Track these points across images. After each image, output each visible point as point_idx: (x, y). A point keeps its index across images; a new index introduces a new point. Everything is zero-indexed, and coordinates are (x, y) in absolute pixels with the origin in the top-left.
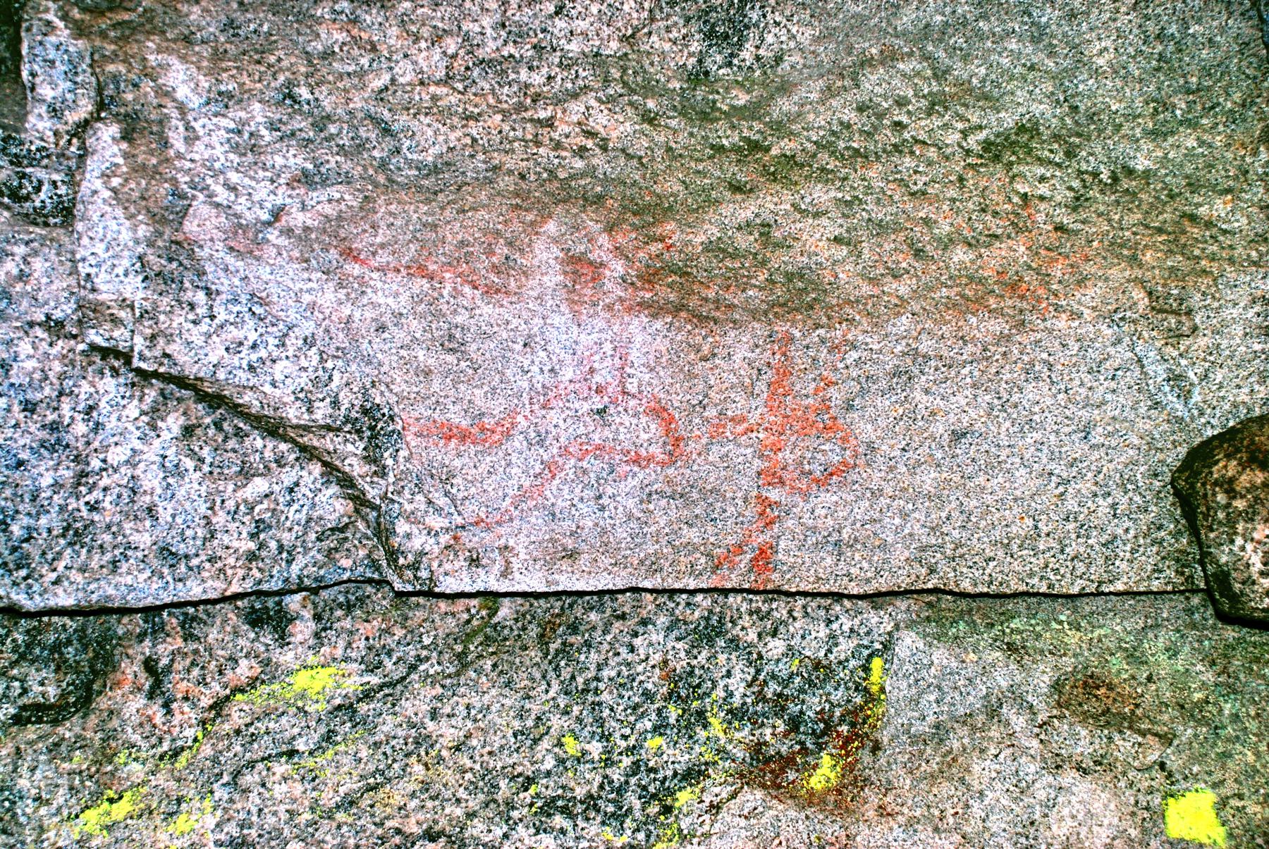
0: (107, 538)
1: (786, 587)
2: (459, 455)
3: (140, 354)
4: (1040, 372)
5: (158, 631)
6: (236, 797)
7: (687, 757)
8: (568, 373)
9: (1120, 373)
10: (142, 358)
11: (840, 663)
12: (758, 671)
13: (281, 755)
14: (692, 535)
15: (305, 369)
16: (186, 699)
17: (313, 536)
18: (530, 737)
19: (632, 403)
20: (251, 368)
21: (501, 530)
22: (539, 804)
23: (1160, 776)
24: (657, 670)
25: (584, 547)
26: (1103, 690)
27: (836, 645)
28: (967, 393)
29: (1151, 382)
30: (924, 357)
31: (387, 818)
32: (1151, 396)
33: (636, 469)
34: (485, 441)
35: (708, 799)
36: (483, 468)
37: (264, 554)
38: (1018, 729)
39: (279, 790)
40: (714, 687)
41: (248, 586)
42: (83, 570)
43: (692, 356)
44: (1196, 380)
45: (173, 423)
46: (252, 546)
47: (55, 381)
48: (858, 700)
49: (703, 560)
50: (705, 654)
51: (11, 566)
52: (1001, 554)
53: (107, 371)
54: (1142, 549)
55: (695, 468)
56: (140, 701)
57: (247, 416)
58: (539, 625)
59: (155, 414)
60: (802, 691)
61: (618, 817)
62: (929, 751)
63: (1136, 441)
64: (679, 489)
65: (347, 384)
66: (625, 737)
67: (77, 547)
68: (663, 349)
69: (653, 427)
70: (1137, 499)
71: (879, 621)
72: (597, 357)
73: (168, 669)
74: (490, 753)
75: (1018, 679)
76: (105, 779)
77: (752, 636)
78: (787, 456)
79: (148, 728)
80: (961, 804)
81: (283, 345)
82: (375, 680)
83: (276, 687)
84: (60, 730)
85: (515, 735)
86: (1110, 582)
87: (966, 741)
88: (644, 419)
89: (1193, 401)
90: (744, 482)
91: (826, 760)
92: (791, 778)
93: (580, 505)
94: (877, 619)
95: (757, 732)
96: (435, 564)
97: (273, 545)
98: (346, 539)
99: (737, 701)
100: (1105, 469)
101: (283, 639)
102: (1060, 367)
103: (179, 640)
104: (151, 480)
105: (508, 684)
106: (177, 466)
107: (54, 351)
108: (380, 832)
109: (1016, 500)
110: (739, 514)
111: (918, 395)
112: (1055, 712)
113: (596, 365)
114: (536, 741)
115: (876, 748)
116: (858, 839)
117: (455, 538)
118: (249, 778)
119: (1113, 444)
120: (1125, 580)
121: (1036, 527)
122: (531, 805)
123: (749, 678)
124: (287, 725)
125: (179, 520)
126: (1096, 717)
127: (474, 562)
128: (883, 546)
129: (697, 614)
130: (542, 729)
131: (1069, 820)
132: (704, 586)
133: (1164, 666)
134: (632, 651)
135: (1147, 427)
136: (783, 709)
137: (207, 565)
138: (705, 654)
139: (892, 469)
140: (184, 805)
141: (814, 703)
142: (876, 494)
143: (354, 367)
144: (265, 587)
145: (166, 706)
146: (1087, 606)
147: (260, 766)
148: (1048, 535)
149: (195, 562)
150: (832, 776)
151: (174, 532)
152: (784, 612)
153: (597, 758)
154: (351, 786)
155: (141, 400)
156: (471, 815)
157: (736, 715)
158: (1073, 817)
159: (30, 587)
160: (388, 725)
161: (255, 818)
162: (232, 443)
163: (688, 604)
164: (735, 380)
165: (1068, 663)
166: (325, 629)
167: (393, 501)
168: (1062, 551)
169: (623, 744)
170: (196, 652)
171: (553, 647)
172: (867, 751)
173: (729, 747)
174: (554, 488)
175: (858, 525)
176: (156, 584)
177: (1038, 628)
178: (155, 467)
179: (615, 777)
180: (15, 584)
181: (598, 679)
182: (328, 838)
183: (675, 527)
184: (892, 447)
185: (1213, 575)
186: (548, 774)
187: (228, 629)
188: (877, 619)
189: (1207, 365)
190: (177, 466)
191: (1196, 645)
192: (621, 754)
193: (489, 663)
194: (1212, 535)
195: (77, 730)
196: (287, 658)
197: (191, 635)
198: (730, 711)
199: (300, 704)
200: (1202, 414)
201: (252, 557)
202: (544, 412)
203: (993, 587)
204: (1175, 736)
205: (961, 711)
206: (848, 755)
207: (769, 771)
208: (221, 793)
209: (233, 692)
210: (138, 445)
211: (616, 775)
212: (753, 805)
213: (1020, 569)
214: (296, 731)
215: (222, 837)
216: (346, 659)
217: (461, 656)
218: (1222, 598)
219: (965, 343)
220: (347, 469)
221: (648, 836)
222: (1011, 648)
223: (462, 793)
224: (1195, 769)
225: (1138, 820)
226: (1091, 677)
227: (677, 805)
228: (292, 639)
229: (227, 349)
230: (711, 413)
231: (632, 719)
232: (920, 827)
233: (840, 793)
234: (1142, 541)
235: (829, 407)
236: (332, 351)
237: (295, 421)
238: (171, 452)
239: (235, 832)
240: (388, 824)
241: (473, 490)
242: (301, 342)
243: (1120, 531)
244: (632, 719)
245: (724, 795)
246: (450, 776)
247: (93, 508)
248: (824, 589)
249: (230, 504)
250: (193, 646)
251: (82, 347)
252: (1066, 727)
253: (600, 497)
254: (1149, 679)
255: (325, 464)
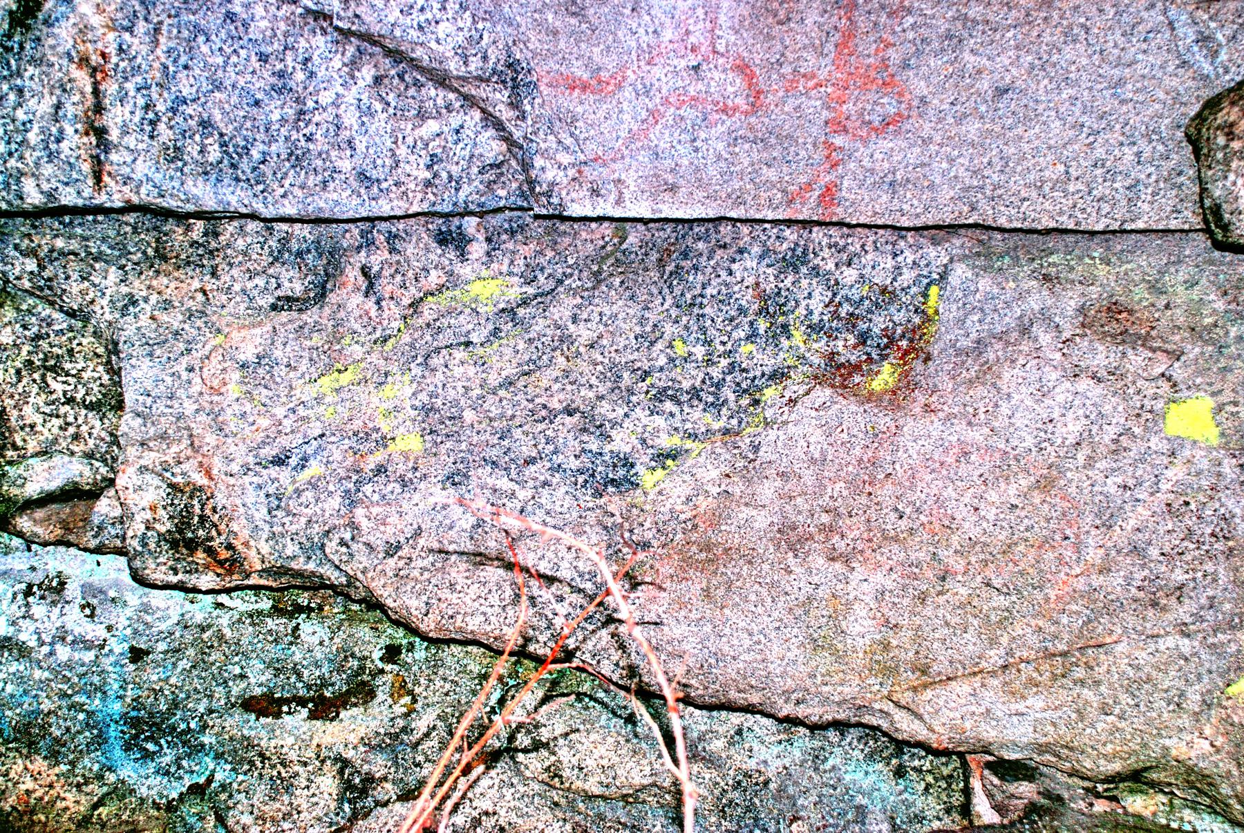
0: (319, 162)
1: (848, 220)
2: (581, 103)
3: (338, 14)
4: (1077, 35)
5: (368, 243)
6: (427, 374)
7: (773, 361)
8: (668, 34)
9: (1151, 35)
10: (340, 18)
11: (903, 289)
12: (834, 295)
13: (459, 344)
14: (771, 174)
15: (461, 29)
16: (392, 298)
17: (475, 170)
18: (648, 339)
19: (721, 61)
20: (421, 28)
21: (613, 166)
22: (654, 392)
23: (1166, 386)
24: (750, 290)
25: (682, 182)
26: (1124, 315)
27: (901, 274)
28: (1010, 53)
29: (1180, 43)
30: (972, 21)
31: (536, 396)
32: (1179, 56)
33: (724, 117)
34: (602, 91)
35: (787, 394)
36: (601, 114)
37: (437, 182)
38: (1044, 344)
39: (458, 371)
40: (797, 305)
41: (425, 207)
42: (302, 187)
43: (770, 20)
44: (1224, 42)
45: (366, 74)
46: (428, 175)
47: (281, 38)
48: (917, 320)
49: (779, 195)
50: (790, 279)
51: (252, 182)
52: (1034, 194)
53: (318, 30)
54: (1162, 192)
55: (773, 117)
56: (358, 298)
57: (422, 70)
58: (658, 252)
59: (354, 65)
60: (870, 311)
61: (717, 406)
62: (970, 361)
63: (1162, 95)
64: (760, 135)
65: (494, 42)
66: (724, 343)
67: (298, 169)
68: (746, 13)
69: (738, 81)
70: (1160, 148)
71: (936, 255)
72: (691, 21)
73: (379, 275)
74: (616, 351)
75: (1049, 302)
76: (334, 355)
77: (831, 266)
78: (849, 107)
79: (366, 319)
80: (992, 404)
81: (445, 9)
82: (531, 290)
83: (457, 293)
84: (304, 317)
85: (636, 338)
86: (1132, 220)
87: (1000, 353)
88: (731, 75)
89: (1219, 60)
90: (814, 130)
91: (886, 368)
92: (857, 381)
93: (678, 147)
94: (935, 253)
95: (831, 344)
96: (564, 193)
97: (444, 175)
98: (502, 174)
99: (815, 318)
100: (1131, 122)
101: (463, 256)
102: (1096, 31)
103: (386, 252)
104: (350, 118)
105: (632, 298)
106: (369, 108)
107: (280, 14)
108: (531, 406)
109: (1050, 148)
110: (810, 157)
111: (967, 56)
112: (1078, 331)
113: (691, 28)
114: (652, 343)
115: (928, 358)
116: (905, 429)
117: (580, 172)
118: (436, 360)
119: (1141, 98)
120: (1146, 219)
121: (1067, 173)
122: (647, 392)
123: (827, 300)
124: (464, 322)
125: (371, 151)
126: (1114, 336)
127: (595, 192)
128: (931, 187)
129: (785, 246)
130: (658, 334)
131: (1083, 419)
132: (781, 217)
133: (1181, 295)
134: (731, 274)
135: (1173, 83)
136: (854, 326)
137: (394, 188)
138: (790, 279)
139: (940, 121)
140: (389, 378)
141: (879, 323)
142: (926, 142)
143: (499, 28)
144: (438, 208)
145: (378, 303)
146: (1119, 245)
147: (444, 352)
148: (1077, 179)
149: (384, 185)
150: (890, 380)
151: (367, 161)
152: (858, 246)
153: (700, 359)
154: (510, 371)
155: (343, 54)
156: (601, 398)
157: (815, 329)
158: (1087, 417)
159: (265, 198)
160: (539, 325)
161: (440, 391)
162: (412, 91)
163: (778, 237)
164: (807, 42)
165: (1094, 292)
166: (494, 249)
167: (532, 141)
168: (1090, 193)
169: (722, 348)
170: (398, 262)
171: (668, 269)
172: (920, 361)
173: (807, 355)
174: (657, 133)
175: (910, 168)
176: (355, 201)
177: (1072, 263)
178: (352, 108)
179: (714, 375)
180: (255, 195)
181: (702, 296)
182: (493, 409)
183: (757, 167)
184: (941, 101)
185: (1210, 208)
186: (661, 369)
187: (421, 245)
188: (935, 253)
189: (1235, 27)
190: (369, 108)
191: (1212, 278)
192: (719, 356)
193: (618, 280)
194: (1210, 173)
195: (316, 317)
196: (465, 271)
197: (395, 249)
198: (809, 326)
199: (473, 306)
200: (1227, 72)
201: (428, 184)
202: (648, 68)
203: (1026, 223)
204: (1183, 353)
205: (999, 329)
206: (905, 364)
207: (839, 374)
208: (417, 371)
209: (426, 295)
210: (341, 90)
211: (716, 373)
212: (823, 400)
213: (1051, 208)
214: (470, 326)
215: (417, 403)
216: (510, 274)
217: (597, 274)
218: (1215, 227)
219: (1010, 9)
220: (498, 114)
221: (740, 422)
222: (1046, 278)
223: (594, 381)
224: (1198, 381)
225: (1142, 420)
226: (1115, 304)
227: (764, 398)
228: (470, 257)
229: (401, 11)
230: (787, 69)
231: (729, 328)
232: (956, 421)
233: (894, 393)
234: (1162, 185)
235: (888, 66)
236: (481, 14)
237: (455, 73)
238: (364, 97)
239: (426, 399)
240: (538, 401)
241: (592, 132)
242: (457, 6)
243: (1143, 176)
244: (729, 328)
245: (801, 392)
246: (585, 367)
247: (309, 139)
248: (879, 222)
249: (410, 141)
250: (396, 258)
251: (300, 10)
252: (1086, 343)
253: (694, 140)
254: (1167, 306)
255: (483, 111)
